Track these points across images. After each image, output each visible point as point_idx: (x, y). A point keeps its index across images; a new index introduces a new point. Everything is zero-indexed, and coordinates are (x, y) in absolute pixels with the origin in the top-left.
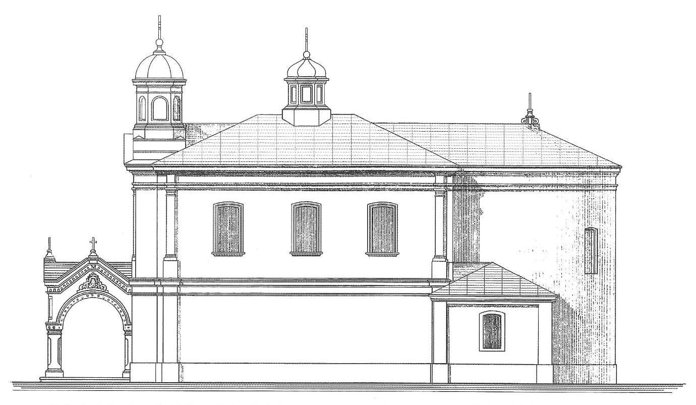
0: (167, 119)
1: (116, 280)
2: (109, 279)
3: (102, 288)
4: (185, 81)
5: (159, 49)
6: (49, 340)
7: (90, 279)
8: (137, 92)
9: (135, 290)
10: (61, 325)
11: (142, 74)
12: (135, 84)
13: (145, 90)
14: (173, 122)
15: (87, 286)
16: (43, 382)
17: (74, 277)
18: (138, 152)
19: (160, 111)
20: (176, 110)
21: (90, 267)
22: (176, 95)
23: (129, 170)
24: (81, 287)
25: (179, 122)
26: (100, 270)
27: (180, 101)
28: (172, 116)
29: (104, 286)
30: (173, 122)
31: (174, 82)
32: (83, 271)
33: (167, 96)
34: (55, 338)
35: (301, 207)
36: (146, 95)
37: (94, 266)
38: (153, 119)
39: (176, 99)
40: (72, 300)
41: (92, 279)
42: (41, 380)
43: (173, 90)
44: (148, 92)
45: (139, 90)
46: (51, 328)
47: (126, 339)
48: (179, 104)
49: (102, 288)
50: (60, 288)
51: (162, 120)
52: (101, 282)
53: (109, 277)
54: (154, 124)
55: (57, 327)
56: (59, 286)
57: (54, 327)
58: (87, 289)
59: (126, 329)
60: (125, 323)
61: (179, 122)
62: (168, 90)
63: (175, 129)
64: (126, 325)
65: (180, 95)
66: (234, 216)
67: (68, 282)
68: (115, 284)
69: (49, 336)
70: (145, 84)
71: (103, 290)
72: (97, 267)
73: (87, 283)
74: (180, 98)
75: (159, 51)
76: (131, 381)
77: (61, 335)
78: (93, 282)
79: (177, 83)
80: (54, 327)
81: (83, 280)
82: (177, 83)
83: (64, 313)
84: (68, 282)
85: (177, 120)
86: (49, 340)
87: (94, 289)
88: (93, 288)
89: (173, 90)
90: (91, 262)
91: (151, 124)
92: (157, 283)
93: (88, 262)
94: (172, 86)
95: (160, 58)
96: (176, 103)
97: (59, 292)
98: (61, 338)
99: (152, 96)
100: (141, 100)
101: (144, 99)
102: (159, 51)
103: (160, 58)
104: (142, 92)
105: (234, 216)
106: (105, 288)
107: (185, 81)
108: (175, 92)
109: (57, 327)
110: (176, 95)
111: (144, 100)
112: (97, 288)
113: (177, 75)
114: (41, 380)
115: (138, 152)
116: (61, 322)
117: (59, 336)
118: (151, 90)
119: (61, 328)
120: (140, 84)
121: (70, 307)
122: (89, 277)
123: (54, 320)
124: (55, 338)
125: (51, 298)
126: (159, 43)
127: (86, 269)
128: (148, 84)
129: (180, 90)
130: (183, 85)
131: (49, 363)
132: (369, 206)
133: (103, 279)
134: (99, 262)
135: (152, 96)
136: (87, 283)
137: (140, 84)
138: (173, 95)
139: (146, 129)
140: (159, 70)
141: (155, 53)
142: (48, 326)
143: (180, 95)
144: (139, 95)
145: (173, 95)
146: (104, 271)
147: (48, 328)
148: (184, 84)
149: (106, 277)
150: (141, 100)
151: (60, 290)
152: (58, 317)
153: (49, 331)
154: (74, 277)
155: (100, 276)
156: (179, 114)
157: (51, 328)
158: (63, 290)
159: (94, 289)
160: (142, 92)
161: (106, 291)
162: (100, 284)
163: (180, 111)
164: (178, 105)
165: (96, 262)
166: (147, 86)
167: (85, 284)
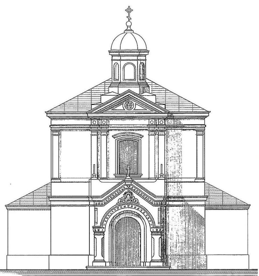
0: (134, 79)
1: (145, 196)
2: (140, 196)
3: (135, 201)
4: (148, 52)
5: (129, 28)
6: (95, 239)
7: (126, 195)
8: (112, 60)
9: (53, 203)
10: (104, 228)
11: (116, 47)
12: (111, 54)
13: (119, 58)
14: (139, 81)
15: (124, 199)
16: (88, 270)
17: (114, 194)
19: (129, 73)
20: (142, 73)
21: (126, 187)
22: (142, 62)
23: (48, 116)
24: (119, 201)
25: (144, 81)
26: (133, 189)
27: (144, 66)
28: (139, 77)
29: (136, 199)
30: (139, 81)
31: (140, 52)
32: (121, 189)
33: (135, 63)
35: (122, 141)
37: (128, 186)
39: (141, 65)
40: (114, 209)
41: (127, 194)
42: (87, 268)
43: (139, 58)
44: (120, 60)
45: (114, 58)
46: (97, 230)
47: (95, 237)
48: (143, 68)
49: (135, 201)
50: (103, 202)
51: (131, 80)
52: (134, 197)
53: (140, 194)
54: (125, 83)
55: (101, 230)
56: (154, 201)
57: (99, 230)
58: (124, 202)
59: (152, 230)
60: (152, 226)
61: (144, 81)
62: (136, 58)
63: (140, 86)
64: (152, 228)
65: (144, 62)
67: (110, 198)
68: (145, 199)
69: (153, 236)
70: (118, 54)
71: (135, 203)
72: (131, 187)
73: (124, 197)
74: (145, 64)
75: (129, 30)
76: (208, 269)
77: (104, 235)
78: (128, 197)
79: (142, 53)
80: (99, 230)
81: (121, 195)
82: (142, 53)
83: (106, 220)
84: (110, 198)
85: (142, 80)
86: (95, 239)
87: (129, 201)
88: (128, 201)
89: (139, 58)
90: (126, 183)
91: (123, 83)
92: (90, 199)
93: (124, 183)
94: (138, 56)
95: (129, 35)
96: (141, 67)
97: (102, 205)
98: (104, 237)
99: (123, 63)
100: (115, 66)
101: (117, 65)
102: (129, 30)
103: (129, 35)
106: (137, 201)
107: (148, 52)
108: (141, 60)
109: (101, 230)
110: (142, 62)
111: (117, 65)
112: (132, 201)
113: (142, 47)
114: (87, 268)
116: (104, 226)
117: (103, 236)
118: (122, 58)
119: (104, 230)
120: (115, 54)
121: (110, 215)
122: (125, 193)
123: (99, 225)
124: (99, 238)
125: (96, 209)
126: (129, 24)
127: (123, 188)
128: (120, 54)
129: (144, 58)
130: (146, 55)
131: (153, 256)
132: (119, 141)
133: (135, 195)
134: (132, 183)
135: (123, 63)
136: (124, 197)
137: (115, 54)
138: (139, 62)
139: (119, 86)
140: (129, 44)
141: (125, 32)
142: (94, 229)
143: (144, 62)
144: (114, 62)
145: (139, 62)
146: (136, 190)
147: (94, 231)
148: (147, 54)
149: (138, 194)
150: (115, 66)
151: (104, 204)
152: (102, 223)
153: (95, 233)
154: (114, 194)
155: (133, 193)
156: (143, 76)
157: (97, 230)
158: (105, 204)
159: (129, 201)
161: (138, 203)
162: (134, 198)
163: (144, 73)
164: (143, 69)
165: (130, 183)
166: (119, 55)
167: (122, 198)
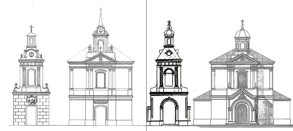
2: (247, 95)
11: (237, 36)
18: (131, 100)
27: (249, 44)
33: (245, 42)
34: (231, 112)
36: (238, 42)
38: (241, 49)
45: (236, 40)
51: (243, 49)
55: (231, 109)
66: (267, 117)
75: (242, 29)
82: (248, 39)
95: (242, 31)
99: (240, 42)
102: (242, 29)
103: (242, 31)
104: (237, 41)
105: (267, 117)
108: (247, 41)
113: (248, 36)
115: (131, 100)
123: (230, 107)
133: (245, 95)
135: (240, 42)
140: (243, 35)
144: (236, 42)
152: (232, 106)
160: (237, 41)
166: (239, 39)
